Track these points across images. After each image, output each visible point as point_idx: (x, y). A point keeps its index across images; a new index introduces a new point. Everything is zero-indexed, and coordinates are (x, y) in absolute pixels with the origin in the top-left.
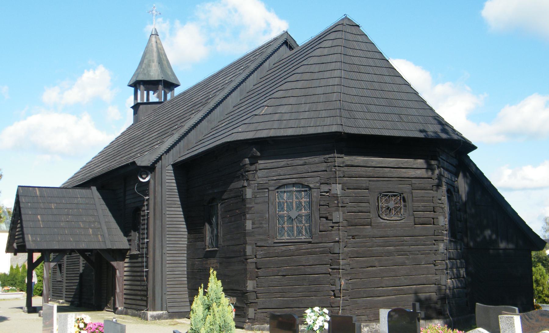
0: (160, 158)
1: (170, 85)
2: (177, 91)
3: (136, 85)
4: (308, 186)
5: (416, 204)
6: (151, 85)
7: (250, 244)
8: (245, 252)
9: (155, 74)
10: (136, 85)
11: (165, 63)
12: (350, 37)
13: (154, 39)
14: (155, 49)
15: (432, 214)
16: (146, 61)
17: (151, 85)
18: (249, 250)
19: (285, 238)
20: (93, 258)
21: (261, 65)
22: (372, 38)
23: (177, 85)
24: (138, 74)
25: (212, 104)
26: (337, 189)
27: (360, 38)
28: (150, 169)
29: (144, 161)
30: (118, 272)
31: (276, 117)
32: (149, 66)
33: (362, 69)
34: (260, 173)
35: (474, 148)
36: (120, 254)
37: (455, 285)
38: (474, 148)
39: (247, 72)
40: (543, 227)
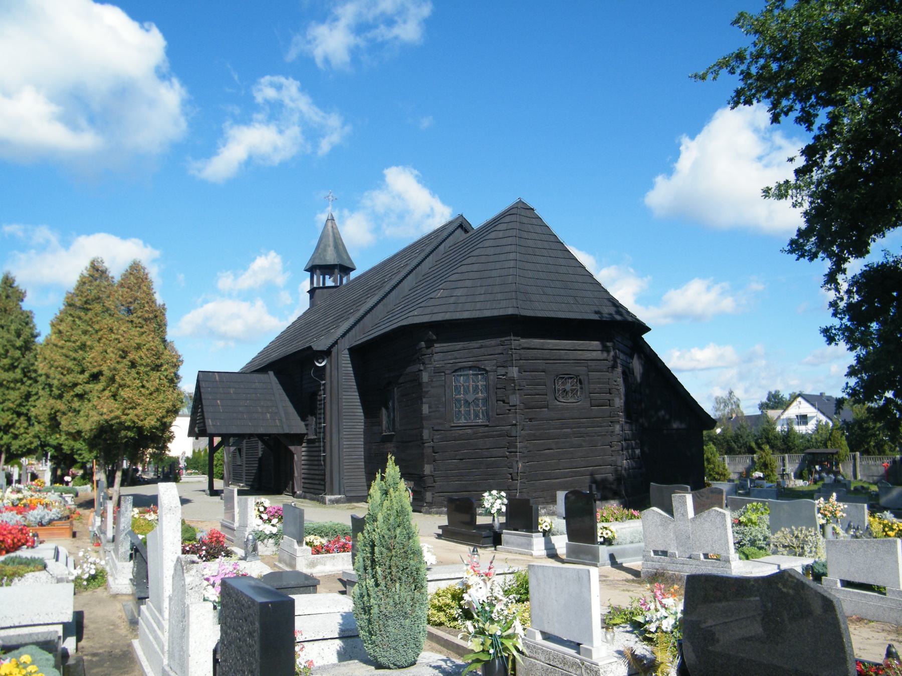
0: (336, 343)
2: (353, 275)
3: (312, 269)
9: (331, 258)
11: (341, 247)
13: (330, 224)
14: (331, 234)
16: (322, 246)
18: (426, 434)
19: (462, 421)
25: (387, 288)
29: (321, 345)
33: (538, 252)
35: (648, 329)
38: (648, 329)
39: (423, 255)
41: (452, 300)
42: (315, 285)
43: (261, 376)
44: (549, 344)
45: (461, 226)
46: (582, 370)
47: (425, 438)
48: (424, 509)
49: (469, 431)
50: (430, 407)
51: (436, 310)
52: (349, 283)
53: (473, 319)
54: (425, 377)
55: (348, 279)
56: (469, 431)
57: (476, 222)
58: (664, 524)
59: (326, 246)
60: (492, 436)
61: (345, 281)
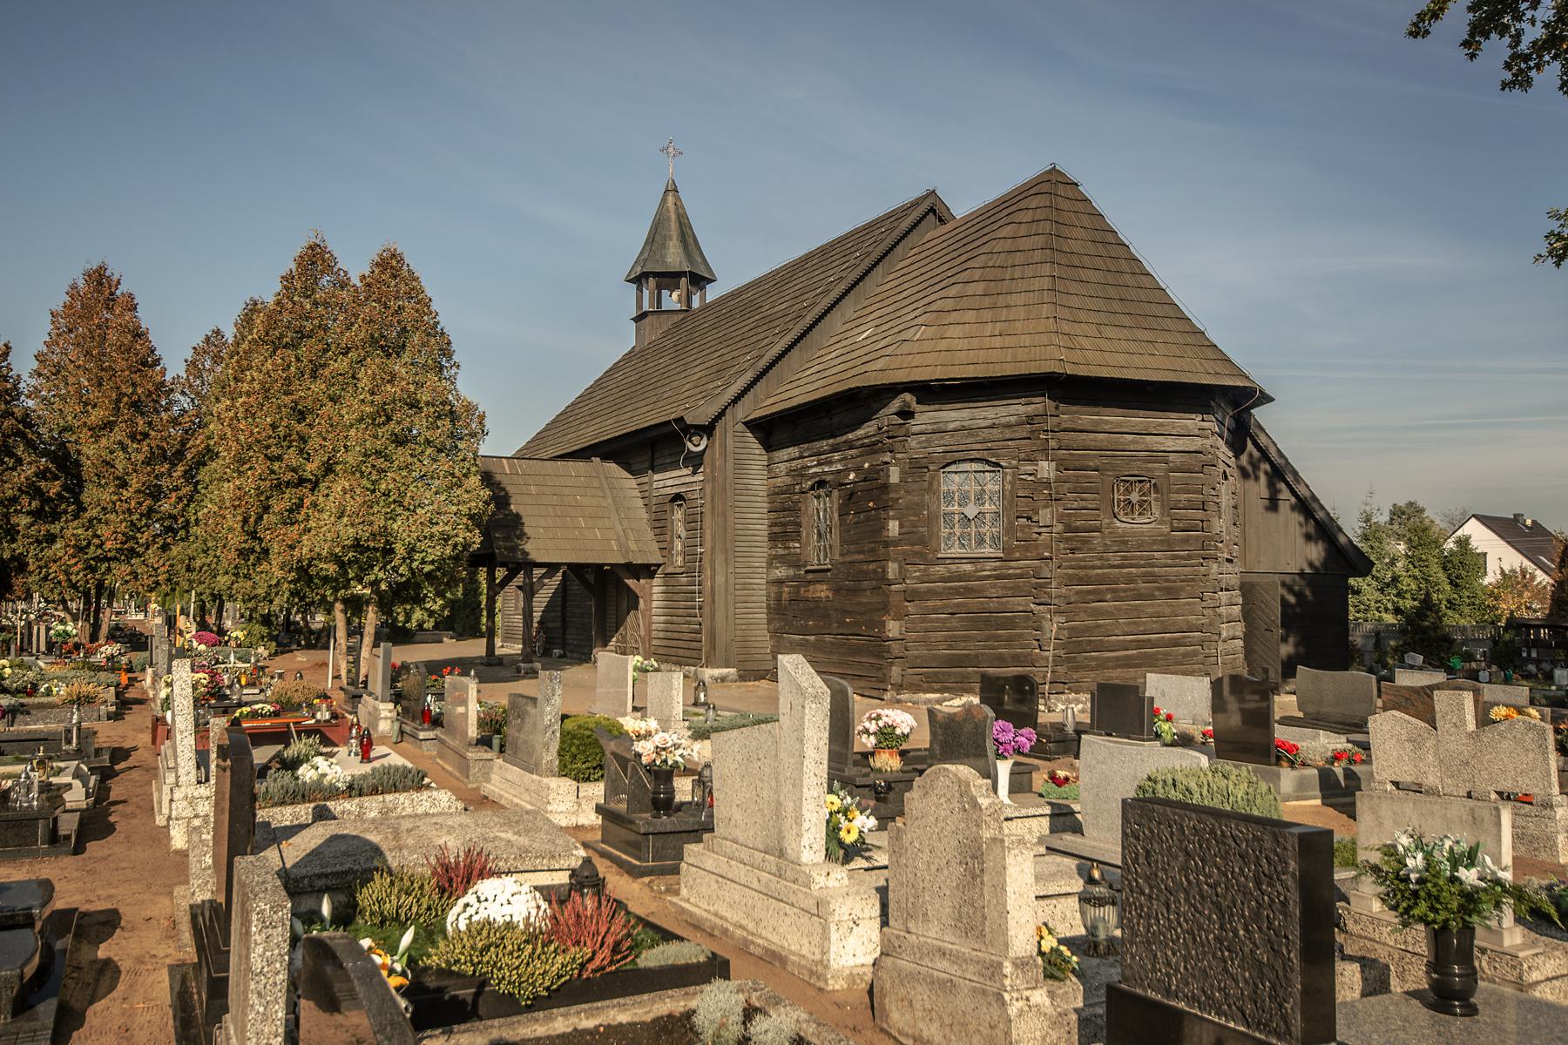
0: (722, 414)
1: (699, 281)
2: (713, 293)
3: (639, 280)
4: (998, 465)
5: (1174, 496)
6: (668, 279)
7: (895, 560)
8: (884, 571)
9: (674, 258)
10: (639, 280)
11: (691, 241)
12: (1064, 205)
13: (670, 198)
14: (673, 217)
15: (1199, 514)
16: (658, 237)
17: (668, 279)
18: (892, 569)
19: (956, 551)
20: (591, 578)
21: (891, 249)
22: (1100, 203)
23: (711, 281)
24: (645, 260)
25: (808, 320)
26: (1046, 469)
27: (1080, 206)
28: (708, 430)
29: (699, 415)
30: (641, 601)
31: (943, 345)
32: (664, 246)
33: (1087, 261)
34: (913, 442)
35: (1266, 399)
36: (647, 571)
37: (893, 587)
38: (1266, 399)
39: (867, 263)
40: (157, 362)
41: (943, 345)
42: (646, 307)
43: (581, 465)
44: (1107, 422)
45: (932, 210)
46: (1159, 469)
47: (891, 576)
48: (887, 696)
49: (968, 567)
50: (901, 526)
51: (918, 360)
52: (705, 308)
53: (1095, 404)
54: (894, 476)
55: (703, 298)
56: (968, 567)
57: (961, 206)
58: (1416, 742)
59: (665, 238)
60: (1008, 577)
61: (696, 304)
